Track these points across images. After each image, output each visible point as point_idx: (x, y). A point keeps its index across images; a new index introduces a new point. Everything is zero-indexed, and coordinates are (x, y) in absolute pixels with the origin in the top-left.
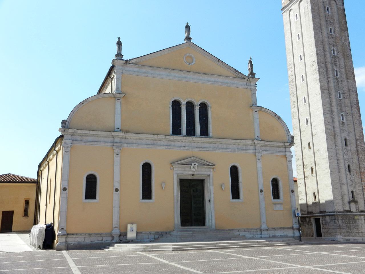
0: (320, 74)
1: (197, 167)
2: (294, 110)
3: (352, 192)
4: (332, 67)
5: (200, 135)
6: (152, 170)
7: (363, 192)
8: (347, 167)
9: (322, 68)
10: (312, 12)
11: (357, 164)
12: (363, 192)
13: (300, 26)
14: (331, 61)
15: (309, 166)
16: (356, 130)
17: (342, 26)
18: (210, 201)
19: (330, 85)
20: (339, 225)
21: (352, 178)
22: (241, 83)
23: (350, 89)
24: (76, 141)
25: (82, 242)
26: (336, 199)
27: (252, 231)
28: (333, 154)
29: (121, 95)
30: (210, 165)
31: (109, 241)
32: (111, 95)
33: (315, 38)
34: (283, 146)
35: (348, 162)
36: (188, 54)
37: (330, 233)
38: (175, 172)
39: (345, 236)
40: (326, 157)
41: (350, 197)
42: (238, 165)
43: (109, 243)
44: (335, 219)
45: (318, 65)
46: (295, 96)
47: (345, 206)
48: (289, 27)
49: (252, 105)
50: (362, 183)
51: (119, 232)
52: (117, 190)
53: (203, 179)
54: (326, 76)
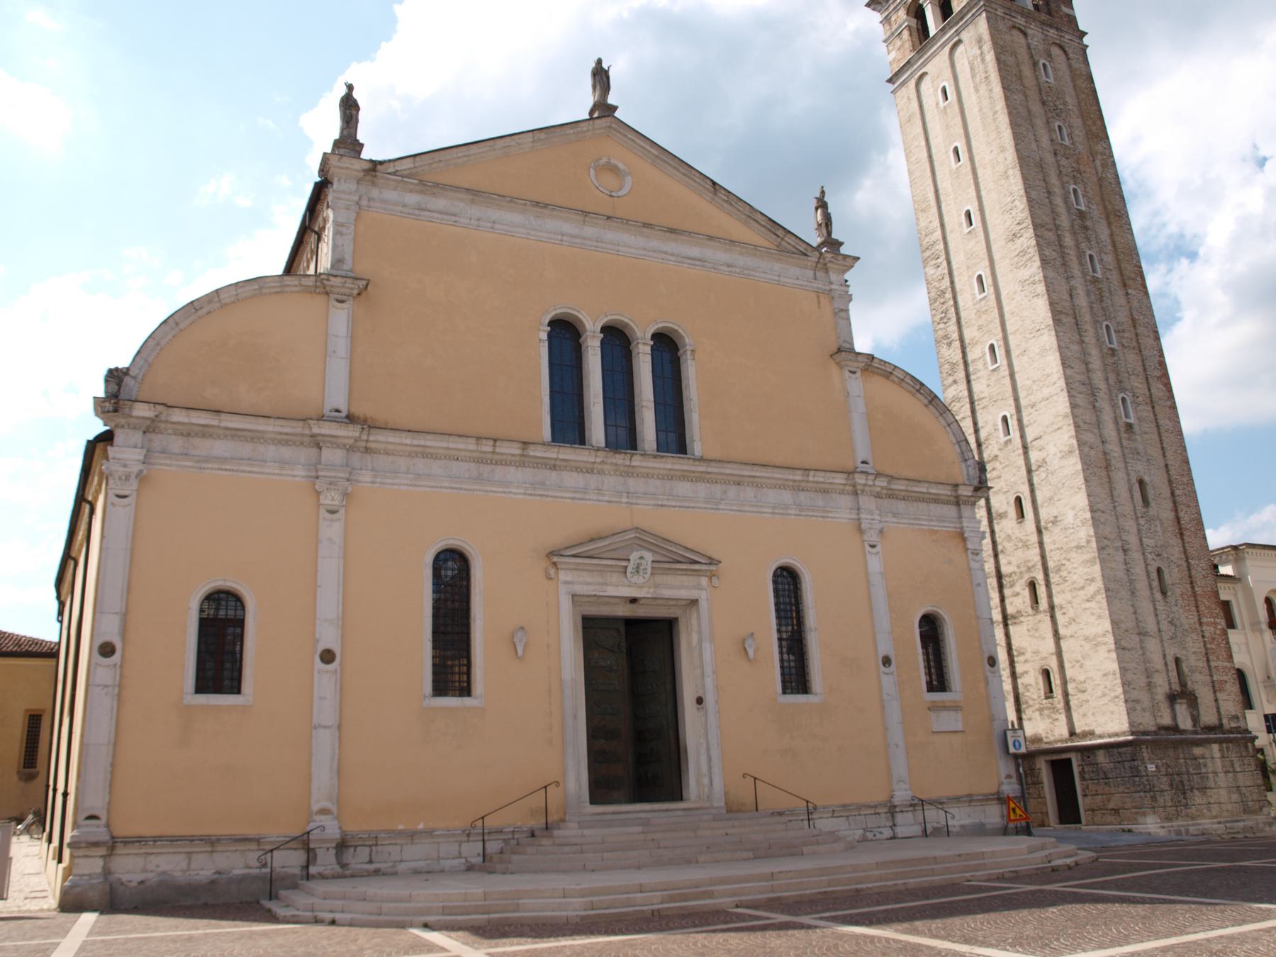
0: (1044, 262)
1: (649, 571)
2: (955, 393)
3: (1177, 661)
4: (1077, 246)
5: (658, 450)
6: (472, 579)
7: (1208, 661)
8: (1154, 575)
9: (1049, 244)
10: (1000, 70)
11: (1181, 565)
12: (1208, 661)
13: (959, 119)
14: (1072, 226)
15: (1022, 578)
16: (1169, 454)
17: (1089, 123)
18: (700, 701)
19: (1076, 302)
20: (1148, 781)
21: (1173, 613)
22: (795, 274)
23: (1137, 317)
25: (178, 874)
26: (1131, 686)
27: (859, 815)
28: (1109, 529)
29: (352, 286)
30: (698, 563)
31: (297, 871)
32: (311, 284)
33: (1017, 150)
35: (1155, 558)
36: (604, 160)
37: (1116, 811)
38: (563, 589)
39: (1168, 819)
40: (1088, 542)
41: (1172, 681)
42: (798, 565)
43: (294, 875)
44: (1134, 760)
45: (1036, 235)
46: (957, 344)
47: (1159, 711)
48: (920, 130)
49: (839, 349)
50: (1202, 631)
51: (338, 831)
52: (328, 656)
53: (672, 616)
54: (1061, 270)
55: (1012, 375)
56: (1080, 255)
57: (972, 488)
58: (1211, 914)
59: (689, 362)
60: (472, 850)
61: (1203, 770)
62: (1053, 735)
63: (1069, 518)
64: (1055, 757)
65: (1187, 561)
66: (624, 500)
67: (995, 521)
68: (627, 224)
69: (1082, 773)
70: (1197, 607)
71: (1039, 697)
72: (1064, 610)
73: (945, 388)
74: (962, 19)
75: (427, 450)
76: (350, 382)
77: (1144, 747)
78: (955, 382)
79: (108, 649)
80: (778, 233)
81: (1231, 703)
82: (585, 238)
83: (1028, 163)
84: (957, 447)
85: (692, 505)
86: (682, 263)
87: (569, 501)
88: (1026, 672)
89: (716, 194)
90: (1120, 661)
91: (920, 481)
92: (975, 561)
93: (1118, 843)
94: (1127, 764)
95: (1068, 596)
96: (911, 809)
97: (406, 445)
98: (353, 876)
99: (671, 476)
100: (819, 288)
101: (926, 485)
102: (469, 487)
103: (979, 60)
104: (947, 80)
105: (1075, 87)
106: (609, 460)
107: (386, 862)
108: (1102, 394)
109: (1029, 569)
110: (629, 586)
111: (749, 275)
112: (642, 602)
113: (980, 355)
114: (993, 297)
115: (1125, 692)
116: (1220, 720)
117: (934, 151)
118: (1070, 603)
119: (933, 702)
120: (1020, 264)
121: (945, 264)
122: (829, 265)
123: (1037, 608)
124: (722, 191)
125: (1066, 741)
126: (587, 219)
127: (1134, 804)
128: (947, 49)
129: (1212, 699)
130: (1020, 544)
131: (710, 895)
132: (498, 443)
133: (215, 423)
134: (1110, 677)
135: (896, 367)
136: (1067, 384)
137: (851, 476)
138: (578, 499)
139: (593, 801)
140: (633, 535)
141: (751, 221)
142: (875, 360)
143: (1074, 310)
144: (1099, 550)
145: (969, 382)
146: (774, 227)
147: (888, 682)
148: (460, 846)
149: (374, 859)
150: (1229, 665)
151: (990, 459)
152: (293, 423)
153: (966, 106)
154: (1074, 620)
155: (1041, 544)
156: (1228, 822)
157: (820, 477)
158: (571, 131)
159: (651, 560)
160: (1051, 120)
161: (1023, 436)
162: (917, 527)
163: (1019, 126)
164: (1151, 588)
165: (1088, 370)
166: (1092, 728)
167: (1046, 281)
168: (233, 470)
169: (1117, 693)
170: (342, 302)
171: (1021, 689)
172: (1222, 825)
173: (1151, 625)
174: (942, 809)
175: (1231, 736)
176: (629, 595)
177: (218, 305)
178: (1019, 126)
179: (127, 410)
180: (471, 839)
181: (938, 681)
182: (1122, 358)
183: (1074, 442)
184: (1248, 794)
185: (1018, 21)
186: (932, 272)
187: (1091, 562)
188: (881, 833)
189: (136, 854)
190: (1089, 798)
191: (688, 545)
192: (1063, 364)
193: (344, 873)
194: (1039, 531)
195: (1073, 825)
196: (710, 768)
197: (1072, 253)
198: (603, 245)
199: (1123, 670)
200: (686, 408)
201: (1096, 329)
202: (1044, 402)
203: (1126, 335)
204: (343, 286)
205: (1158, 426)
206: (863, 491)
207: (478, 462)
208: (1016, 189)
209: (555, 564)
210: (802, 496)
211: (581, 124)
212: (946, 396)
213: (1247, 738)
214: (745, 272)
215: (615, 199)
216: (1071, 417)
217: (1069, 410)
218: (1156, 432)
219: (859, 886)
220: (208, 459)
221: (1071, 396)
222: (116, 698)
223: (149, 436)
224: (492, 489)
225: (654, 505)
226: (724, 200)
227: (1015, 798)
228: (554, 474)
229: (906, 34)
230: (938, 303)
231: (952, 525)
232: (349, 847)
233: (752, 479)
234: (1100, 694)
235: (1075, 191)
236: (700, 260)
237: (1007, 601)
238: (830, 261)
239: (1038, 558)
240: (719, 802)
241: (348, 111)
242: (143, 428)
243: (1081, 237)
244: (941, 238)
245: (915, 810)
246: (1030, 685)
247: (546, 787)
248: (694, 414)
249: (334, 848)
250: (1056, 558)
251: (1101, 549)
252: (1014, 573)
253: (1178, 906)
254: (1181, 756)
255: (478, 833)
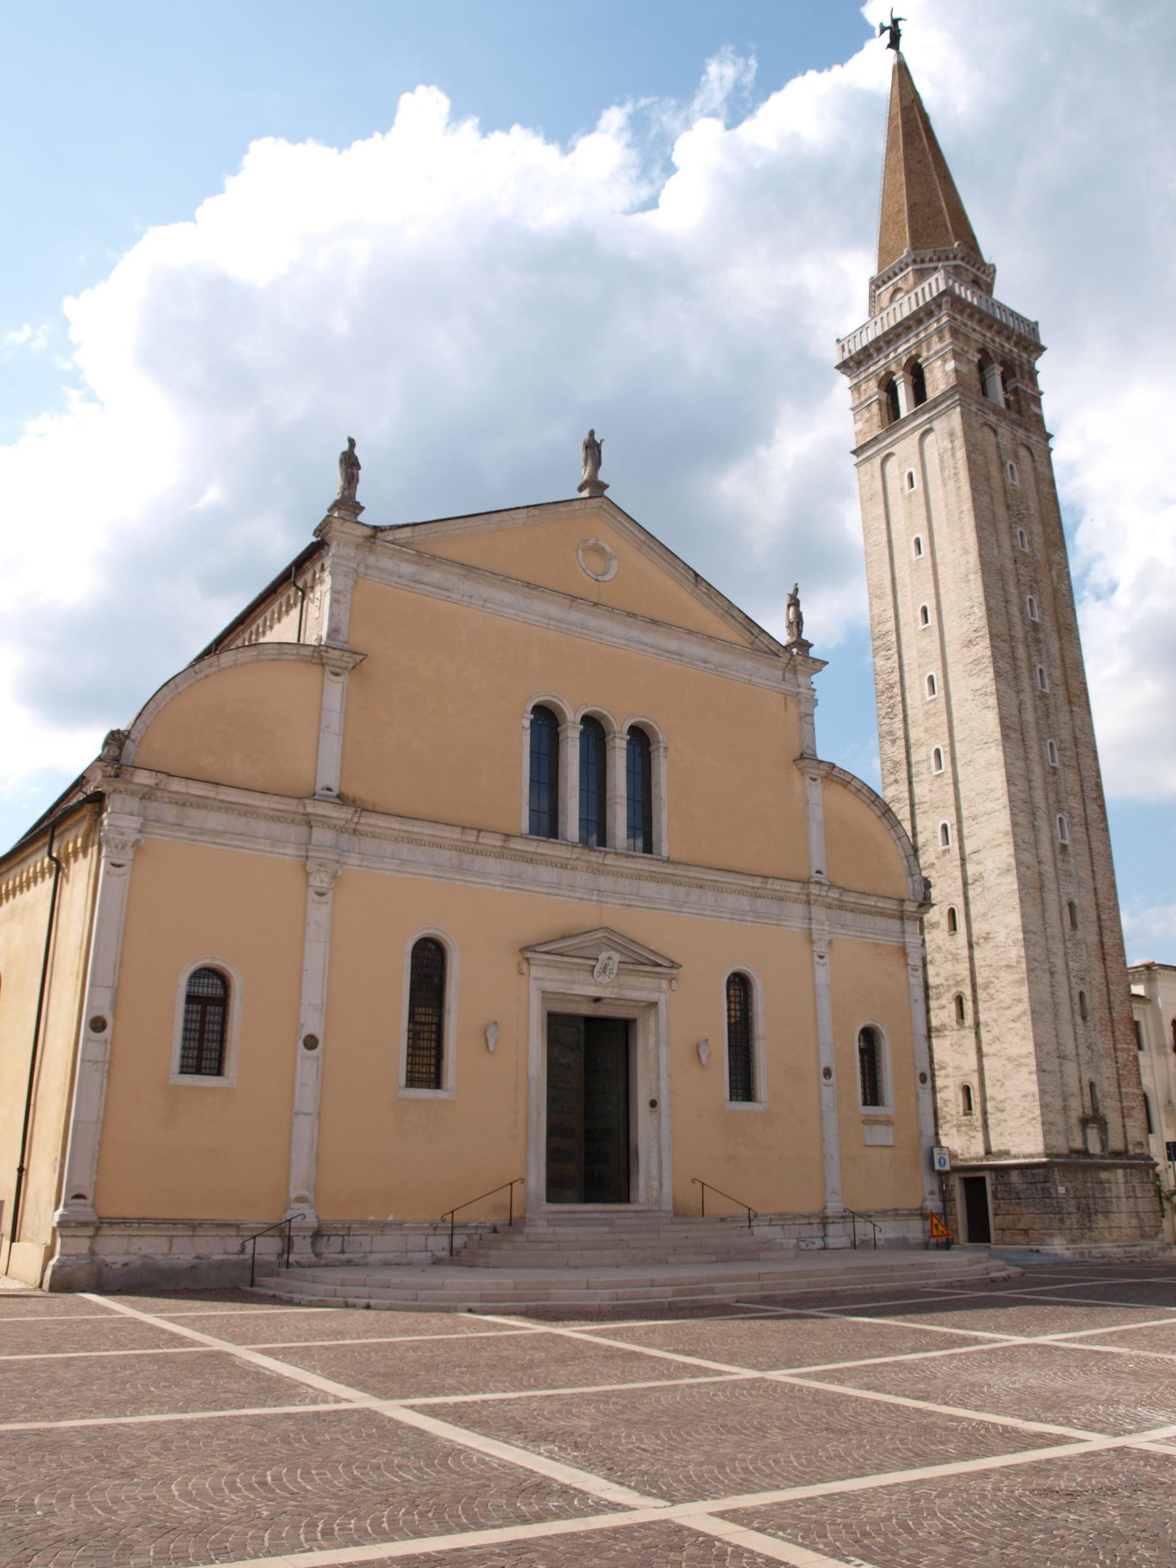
0: (998, 674)
1: (615, 971)
2: (895, 793)
4: (1029, 658)
7: (1119, 1086)
8: (1076, 999)
10: (970, 469)
12: (1119, 1086)
13: (923, 510)
14: (1026, 638)
15: (949, 991)
16: (1098, 877)
17: (1049, 530)
18: (653, 1104)
19: (1024, 717)
22: (766, 673)
24: (158, 824)
25: (160, 1257)
26: (1049, 1109)
29: (349, 659)
30: (660, 965)
31: (273, 1258)
32: (308, 654)
33: (981, 556)
34: (897, 913)
36: (592, 541)
37: (1025, 1232)
38: (534, 985)
39: (1073, 1241)
40: (1018, 962)
43: (270, 1263)
44: (1046, 1182)
45: (992, 646)
46: (902, 742)
48: (881, 512)
49: (802, 755)
50: (1116, 1057)
51: (315, 1220)
52: (311, 1042)
53: (631, 1016)
55: (956, 783)
56: (1031, 668)
57: (917, 904)
58: (1136, 1313)
59: (662, 760)
60: (439, 1244)
61: (1108, 1195)
62: (969, 1153)
63: (1001, 936)
64: (969, 1175)
65: (1107, 986)
66: (595, 898)
67: (926, 931)
68: (612, 611)
69: (995, 1192)
70: (1113, 1032)
71: (958, 1113)
72: (989, 1028)
73: (886, 786)
74: (935, 407)
75: (414, 836)
76: (342, 759)
77: (1056, 1169)
78: (896, 781)
79: (100, 1024)
80: (753, 630)
81: (1137, 1130)
82: (570, 624)
83: (991, 571)
84: (905, 861)
85: (657, 906)
86: (661, 655)
87: (543, 896)
88: (946, 1087)
89: (697, 586)
90: (1041, 1083)
91: (869, 895)
92: (914, 977)
93: (1032, 1263)
94: (1039, 1186)
95: (994, 1014)
96: (842, 1220)
97: (394, 829)
98: (326, 1266)
99: (639, 876)
100: (786, 690)
101: (875, 898)
102: (450, 876)
103: (949, 453)
104: (914, 466)
105: (1038, 491)
106: (584, 857)
107: (356, 1253)
108: (1042, 813)
109: (957, 983)
110: (595, 985)
111: (723, 672)
112: (604, 1001)
113: (925, 758)
114: (943, 701)
115: (1042, 1115)
116: (1126, 1146)
117: (894, 536)
118: (995, 1021)
119: (868, 1115)
120: (973, 672)
121: (896, 657)
122: (799, 667)
123: (963, 1023)
124: (704, 584)
125: (981, 1159)
126: (574, 604)
127: (1043, 1225)
128: (917, 434)
129: (1121, 1124)
130: (950, 957)
131: (711, 1291)
132: (482, 834)
133: (212, 794)
134: (1030, 1098)
135: (854, 777)
136: (1010, 801)
137: (806, 886)
138: (552, 894)
139: (550, 1199)
140: (602, 935)
141: (729, 617)
142: (836, 769)
143: (1021, 725)
144: (1028, 971)
145: (910, 783)
146: (750, 625)
147: (827, 1094)
148: (426, 1239)
149: (346, 1250)
150: (1138, 1092)
151: (926, 865)
152: (289, 801)
153: (932, 498)
154: (998, 1039)
155: (971, 959)
156: (1126, 1246)
157: (778, 885)
158: (563, 509)
159: (617, 961)
160: (1014, 525)
161: (961, 848)
162: (862, 939)
163: (984, 529)
164: (1073, 1012)
165: (1030, 788)
166: (1007, 1148)
167: (998, 695)
168: (225, 845)
169: (1035, 1115)
170: (337, 674)
171: (940, 1104)
172: (1121, 1249)
173: (1070, 1049)
174: (870, 1222)
175: (1135, 1162)
176: (595, 995)
177: (216, 669)
178: (984, 529)
179: (128, 776)
180: (438, 1232)
181: (872, 1094)
182: (1062, 777)
183: (1012, 861)
184: (1146, 1220)
185: (990, 418)
186: (882, 663)
187: (1019, 982)
188: (813, 1243)
189: (120, 1236)
190: (1000, 1217)
191: (652, 948)
192: (1008, 781)
193: (319, 1262)
194: (971, 946)
195: (983, 1244)
196: (660, 1171)
197: (1023, 665)
198: (587, 632)
199: (1042, 1092)
200: (654, 806)
201: (1040, 746)
202: (986, 817)
203: (1068, 753)
204: (340, 660)
205: (1090, 848)
206: (815, 901)
207: (460, 851)
208: (975, 595)
209: (527, 959)
210: (759, 902)
211: (575, 503)
212: (887, 794)
213: (1146, 1165)
214: (720, 669)
215: (602, 584)
216: (1011, 836)
217: (1009, 828)
218: (1088, 855)
219: (835, 1288)
220: (202, 831)
221: (1013, 814)
222: (106, 1075)
223: (148, 803)
224: (472, 879)
225: (622, 905)
226: (704, 593)
227: (937, 1214)
228: (530, 867)
229: (875, 408)
230: (885, 696)
231: (894, 939)
232: (323, 1236)
233: (714, 884)
234: (1018, 1115)
235: (1031, 600)
236: (677, 654)
237: (932, 1013)
238: (800, 664)
239: (967, 973)
240: (667, 1206)
241: (349, 470)
242: (140, 795)
243: (1033, 649)
244: (894, 630)
245: (845, 1222)
246: (949, 1100)
247: (511, 1184)
248: (663, 813)
249: (311, 1237)
250: (985, 975)
251: (1030, 970)
252: (942, 985)
253: (1109, 1308)
254: (1089, 1180)
255: (447, 1227)
